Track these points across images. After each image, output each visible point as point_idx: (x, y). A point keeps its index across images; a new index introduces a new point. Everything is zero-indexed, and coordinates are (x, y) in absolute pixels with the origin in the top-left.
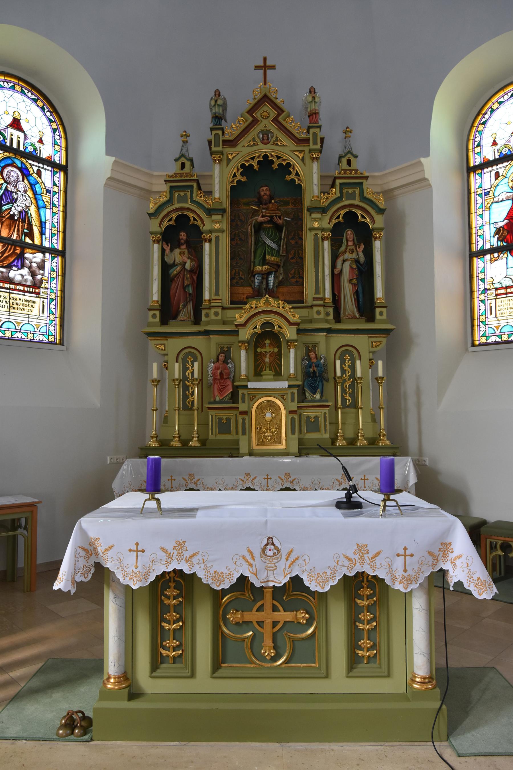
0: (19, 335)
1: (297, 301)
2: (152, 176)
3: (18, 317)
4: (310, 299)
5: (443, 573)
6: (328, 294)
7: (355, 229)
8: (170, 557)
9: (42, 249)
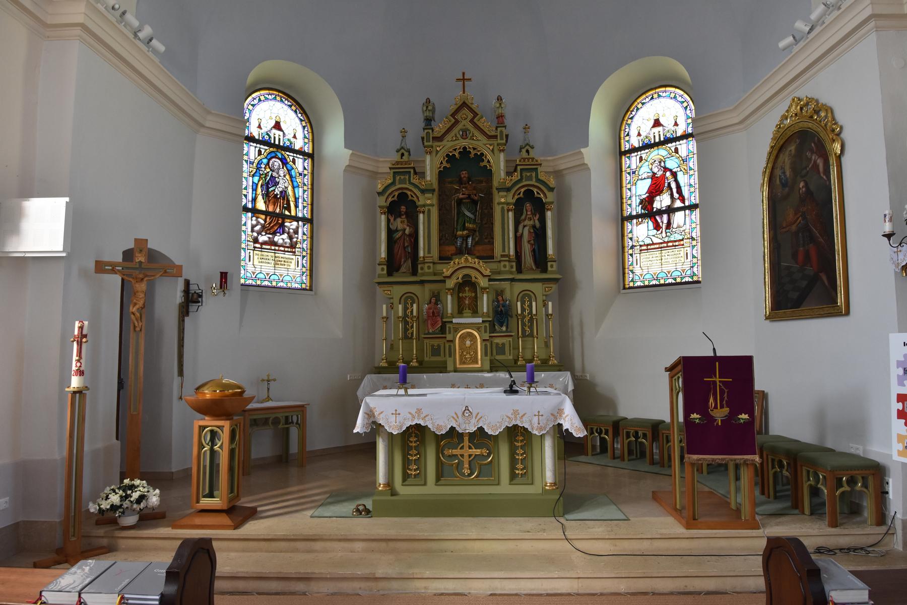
0: (281, 284)
1: (488, 257)
2: (378, 161)
3: (281, 271)
4: (499, 256)
5: (560, 425)
6: (512, 252)
7: (531, 203)
8: (414, 417)
9: (296, 219)
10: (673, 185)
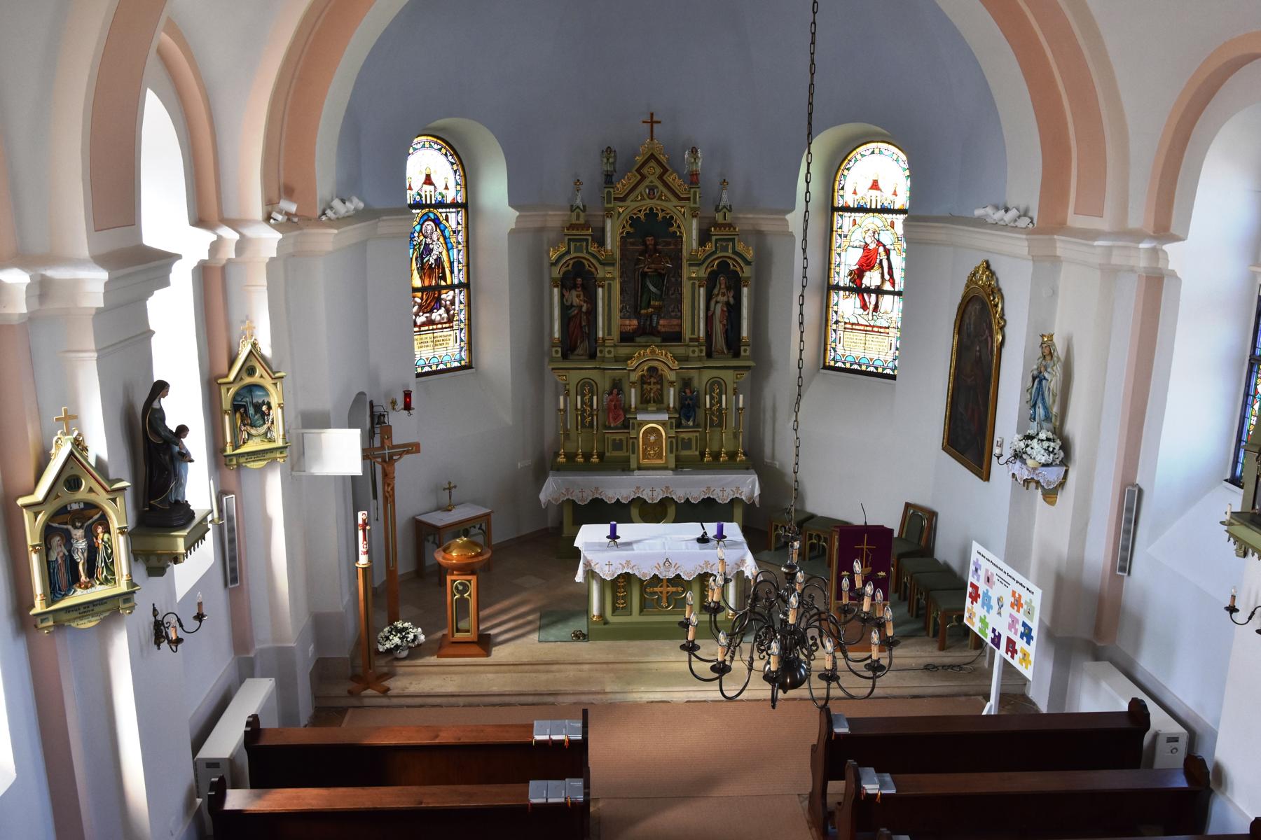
3: (440, 351)
9: (452, 287)
10: (885, 264)
